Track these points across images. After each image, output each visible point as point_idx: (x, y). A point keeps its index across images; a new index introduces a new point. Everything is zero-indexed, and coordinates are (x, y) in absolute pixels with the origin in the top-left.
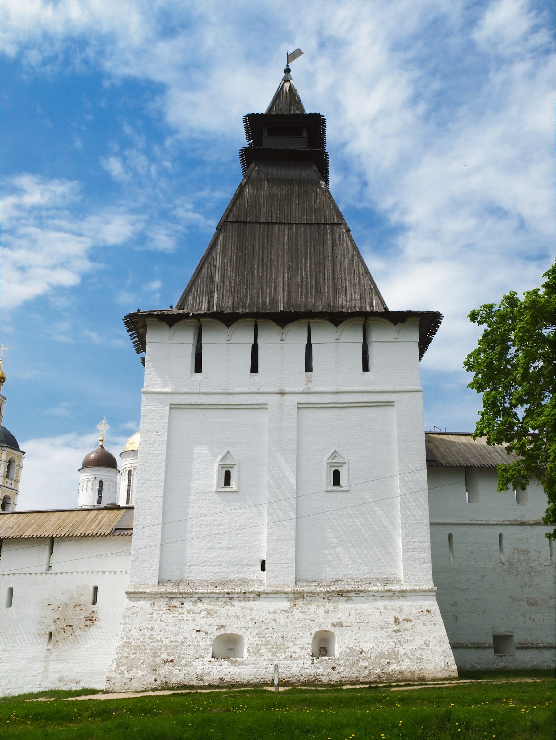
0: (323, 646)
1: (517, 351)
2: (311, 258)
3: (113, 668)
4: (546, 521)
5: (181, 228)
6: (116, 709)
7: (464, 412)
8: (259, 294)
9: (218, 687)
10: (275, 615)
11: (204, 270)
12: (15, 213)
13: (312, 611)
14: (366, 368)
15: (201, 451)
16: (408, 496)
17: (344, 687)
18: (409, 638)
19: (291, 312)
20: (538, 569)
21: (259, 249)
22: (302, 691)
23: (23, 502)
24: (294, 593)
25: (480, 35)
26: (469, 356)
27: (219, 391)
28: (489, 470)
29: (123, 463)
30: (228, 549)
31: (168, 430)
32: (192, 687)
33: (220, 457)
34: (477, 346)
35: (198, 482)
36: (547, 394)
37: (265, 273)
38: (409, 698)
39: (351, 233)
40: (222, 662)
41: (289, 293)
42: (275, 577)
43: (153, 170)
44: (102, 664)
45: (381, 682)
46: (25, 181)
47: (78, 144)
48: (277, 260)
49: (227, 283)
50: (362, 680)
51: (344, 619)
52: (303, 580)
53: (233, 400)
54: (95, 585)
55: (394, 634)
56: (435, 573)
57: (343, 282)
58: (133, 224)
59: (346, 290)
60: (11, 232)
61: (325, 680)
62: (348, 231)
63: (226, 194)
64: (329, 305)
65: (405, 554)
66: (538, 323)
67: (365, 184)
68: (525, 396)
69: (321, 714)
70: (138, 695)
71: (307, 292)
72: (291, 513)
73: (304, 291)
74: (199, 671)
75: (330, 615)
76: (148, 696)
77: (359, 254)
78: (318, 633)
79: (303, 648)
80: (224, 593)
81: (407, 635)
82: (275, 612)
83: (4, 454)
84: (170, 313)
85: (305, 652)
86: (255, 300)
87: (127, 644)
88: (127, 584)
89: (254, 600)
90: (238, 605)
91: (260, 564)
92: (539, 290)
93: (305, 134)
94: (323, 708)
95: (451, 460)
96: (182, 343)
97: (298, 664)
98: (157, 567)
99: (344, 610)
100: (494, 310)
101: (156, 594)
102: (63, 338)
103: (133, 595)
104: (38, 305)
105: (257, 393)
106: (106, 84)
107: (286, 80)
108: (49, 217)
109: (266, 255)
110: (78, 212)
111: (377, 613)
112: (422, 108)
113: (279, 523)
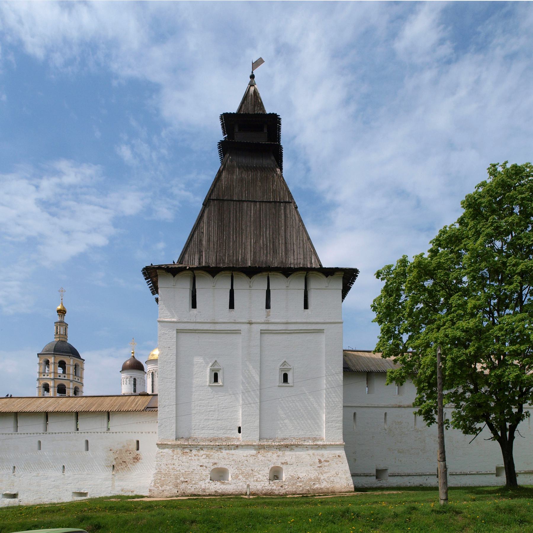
0: (275, 475)
1: (406, 297)
2: (270, 228)
3: (153, 484)
5: (176, 203)
6: (156, 506)
8: (234, 254)
11: (196, 235)
13: (269, 456)
14: (306, 307)
15: (198, 360)
16: (330, 389)
17: (288, 496)
19: (256, 267)
20: (406, 433)
21: (233, 220)
22: (263, 498)
23: (87, 391)
24: (258, 446)
25: (400, 46)
26: (375, 301)
27: (209, 321)
28: (382, 374)
29: (148, 368)
30: (218, 420)
32: (199, 495)
33: (211, 364)
34: (380, 294)
35: (197, 379)
36: (423, 326)
37: (238, 238)
38: (325, 501)
39: (298, 209)
41: (255, 253)
42: (247, 437)
43: (154, 155)
46: (63, 165)
48: (246, 228)
49: (212, 245)
50: (298, 493)
51: (288, 461)
52: (264, 439)
55: (318, 469)
56: (344, 435)
57: (292, 246)
59: (294, 252)
60: (57, 204)
61: (277, 492)
62: (296, 208)
64: (282, 262)
66: (421, 277)
67: (308, 170)
68: (409, 327)
69: (275, 509)
71: (267, 253)
72: (256, 399)
73: (265, 252)
74: (203, 487)
75: (280, 458)
77: (303, 225)
78: (272, 468)
80: (216, 445)
81: (326, 469)
84: (173, 266)
85: (265, 478)
87: (159, 472)
88: (156, 439)
89: (234, 449)
90: (224, 452)
92: (424, 254)
93: (265, 131)
95: (359, 368)
97: (261, 483)
99: (289, 456)
100: (392, 269)
101: (175, 445)
103: (161, 446)
105: (234, 323)
106: (115, 83)
109: (238, 225)
111: (308, 457)
112: (353, 108)
113: (249, 405)
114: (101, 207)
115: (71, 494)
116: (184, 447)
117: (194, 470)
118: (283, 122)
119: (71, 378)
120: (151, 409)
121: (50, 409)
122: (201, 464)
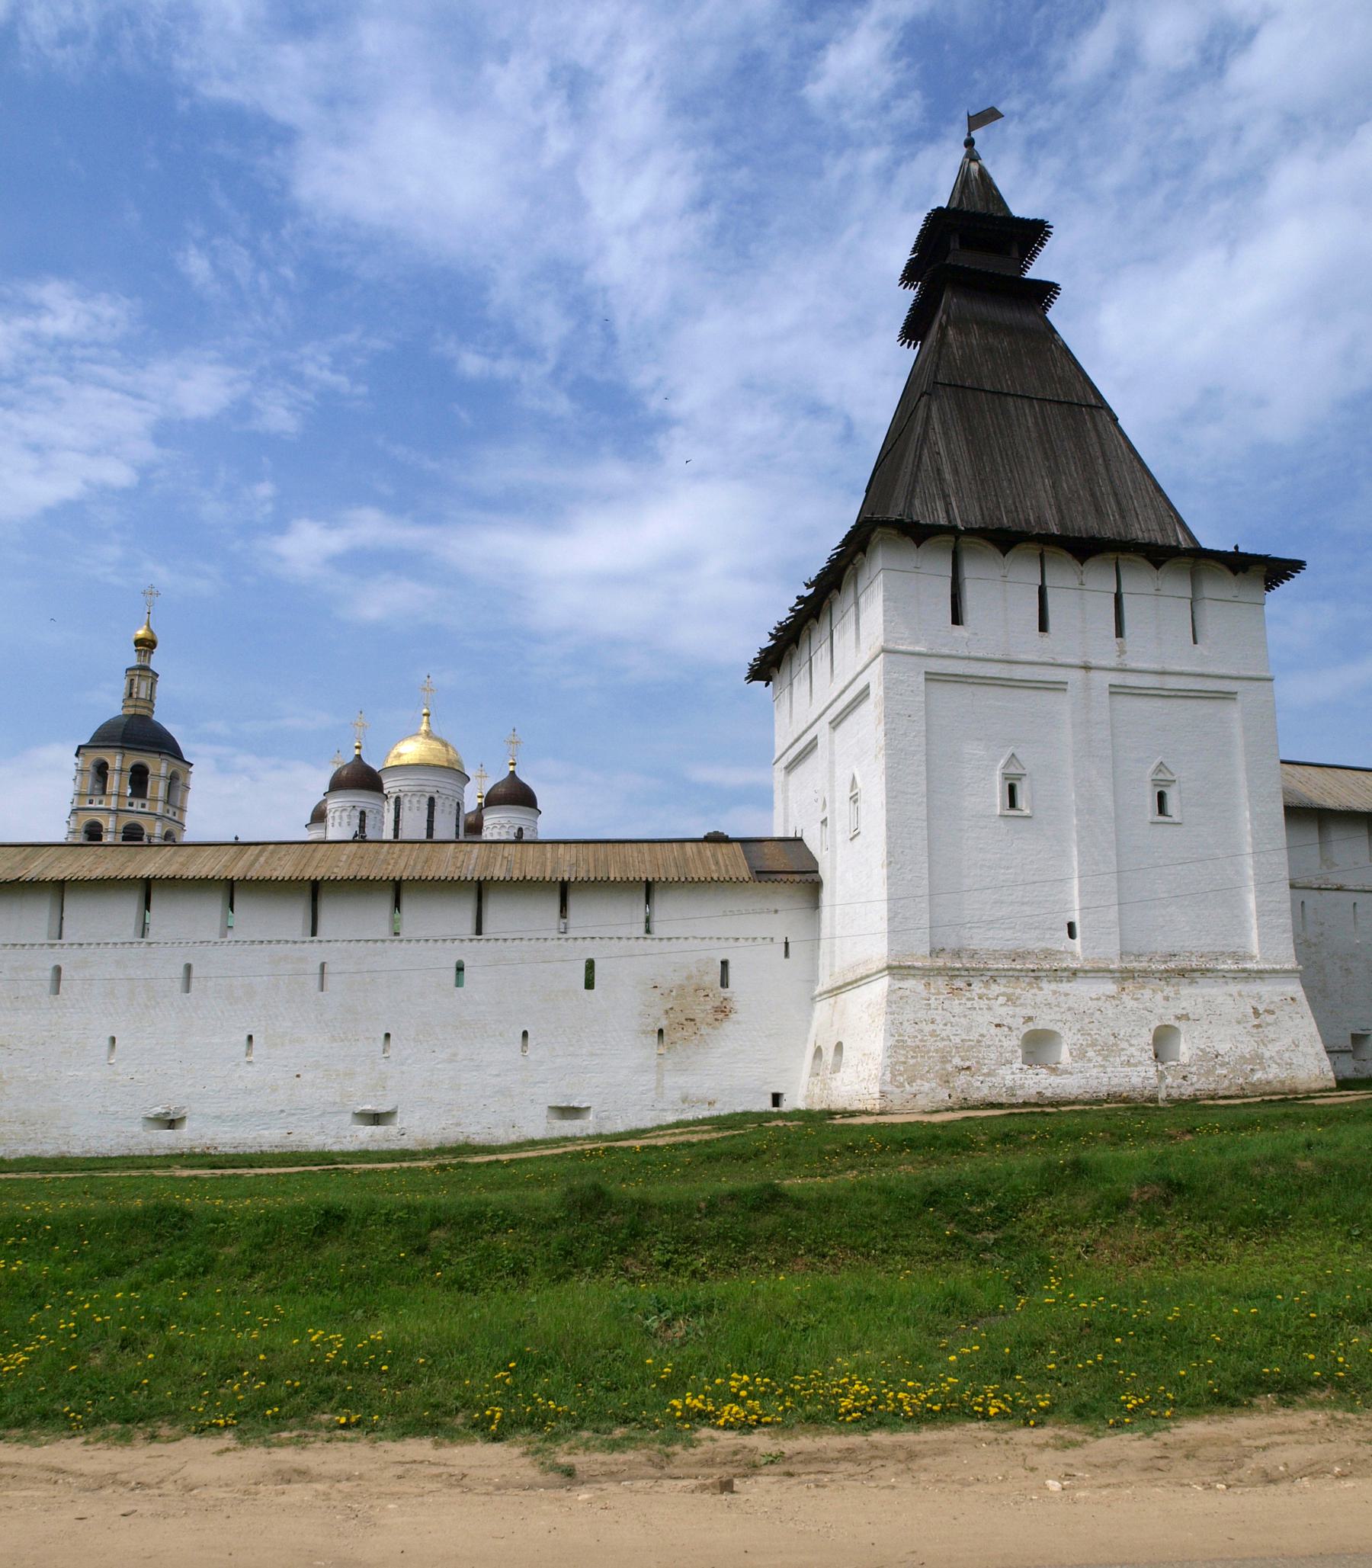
3: (888, 1077)
10: (1100, 1003)
18: (1273, 1036)
25: (817, 92)
27: (997, 656)
29: (389, 784)
31: (927, 713)
33: (1002, 762)
46: (51, 291)
51: (1189, 1010)
53: (1019, 672)
54: (724, 957)
60: (17, 380)
62: (1115, 419)
74: (1009, 1083)
75: (1171, 1003)
79: (1142, 1050)
80: (1027, 970)
81: (1271, 1032)
82: (1098, 999)
85: (1145, 1056)
90: (1048, 987)
97: (1133, 1073)
99: (1190, 997)
104: (69, 517)
108: (83, 360)
110: (133, 351)
112: (712, 217)
114: (128, 393)
115: (546, 1112)
116: (951, 974)
117: (982, 1036)
118: (1050, 242)
119: (159, 808)
120: (773, 877)
121: (499, 872)
122: (997, 1021)
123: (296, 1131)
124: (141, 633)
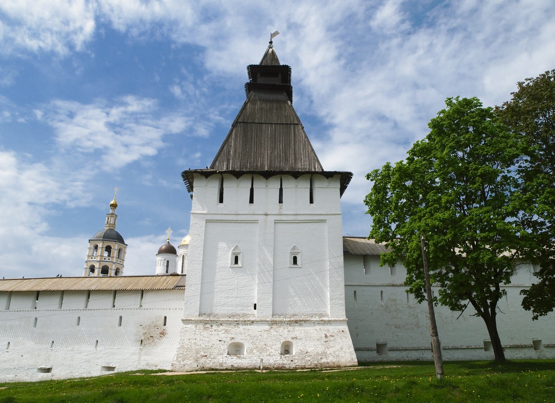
0: (286, 350)
4: (406, 284)
6: (177, 380)
7: (363, 227)
9: (231, 370)
11: (225, 148)
12: (124, 116)
14: (311, 201)
15: (222, 245)
17: (298, 371)
22: (275, 372)
23: (126, 271)
25: (374, 24)
26: (366, 197)
27: (232, 213)
28: (376, 257)
29: (180, 252)
30: (236, 297)
32: (217, 370)
33: (233, 248)
36: (408, 217)
40: (233, 357)
41: (271, 160)
43: (197, 92)
44: (169, 356)
45: (317, 368)
46: (129, 99)
47: (157, 79)
53: (240, 218)
56: (347, 311)
58: (186, 122)
60: (121, 126)
61: (287, 367)
63: (237, 106)
64: (292, 167)
65: (331, 302)
66: (402, 179)
67: (312, 102)
69: (286, 384)
70: (188, 373)
74: (220, 362)
75: (291, 333)
76: (194, 374)
77: (308, 140)
79: (276, 350)
80: (234, 321)
81: (331, 344)
83: (117, 245)
84: (207, 171)
85: (277, 352)
86: (252, 164)
87: (182, 347)
88: (183, 315)
90: (241, 327)
91: (253, 306)
93: (280, 76)
94: (287, 381)
95: (356, 252)
96: (213, 187)
97: (273, 358)
98: (198, 306)
99: (298, 331)
100: (379, 172)
101: (198, 321)
102: (148, 184)
103: (186, 321)
104: (135, 165)
106: (173, 46)
107: (270, 47)
108: (141, 118)
110: (156, 115)
111: (315, 332)
112: (343, 62)
116: (205, 323)
117: (213, 344)
123: (18, 375)
124: (112, 202)
